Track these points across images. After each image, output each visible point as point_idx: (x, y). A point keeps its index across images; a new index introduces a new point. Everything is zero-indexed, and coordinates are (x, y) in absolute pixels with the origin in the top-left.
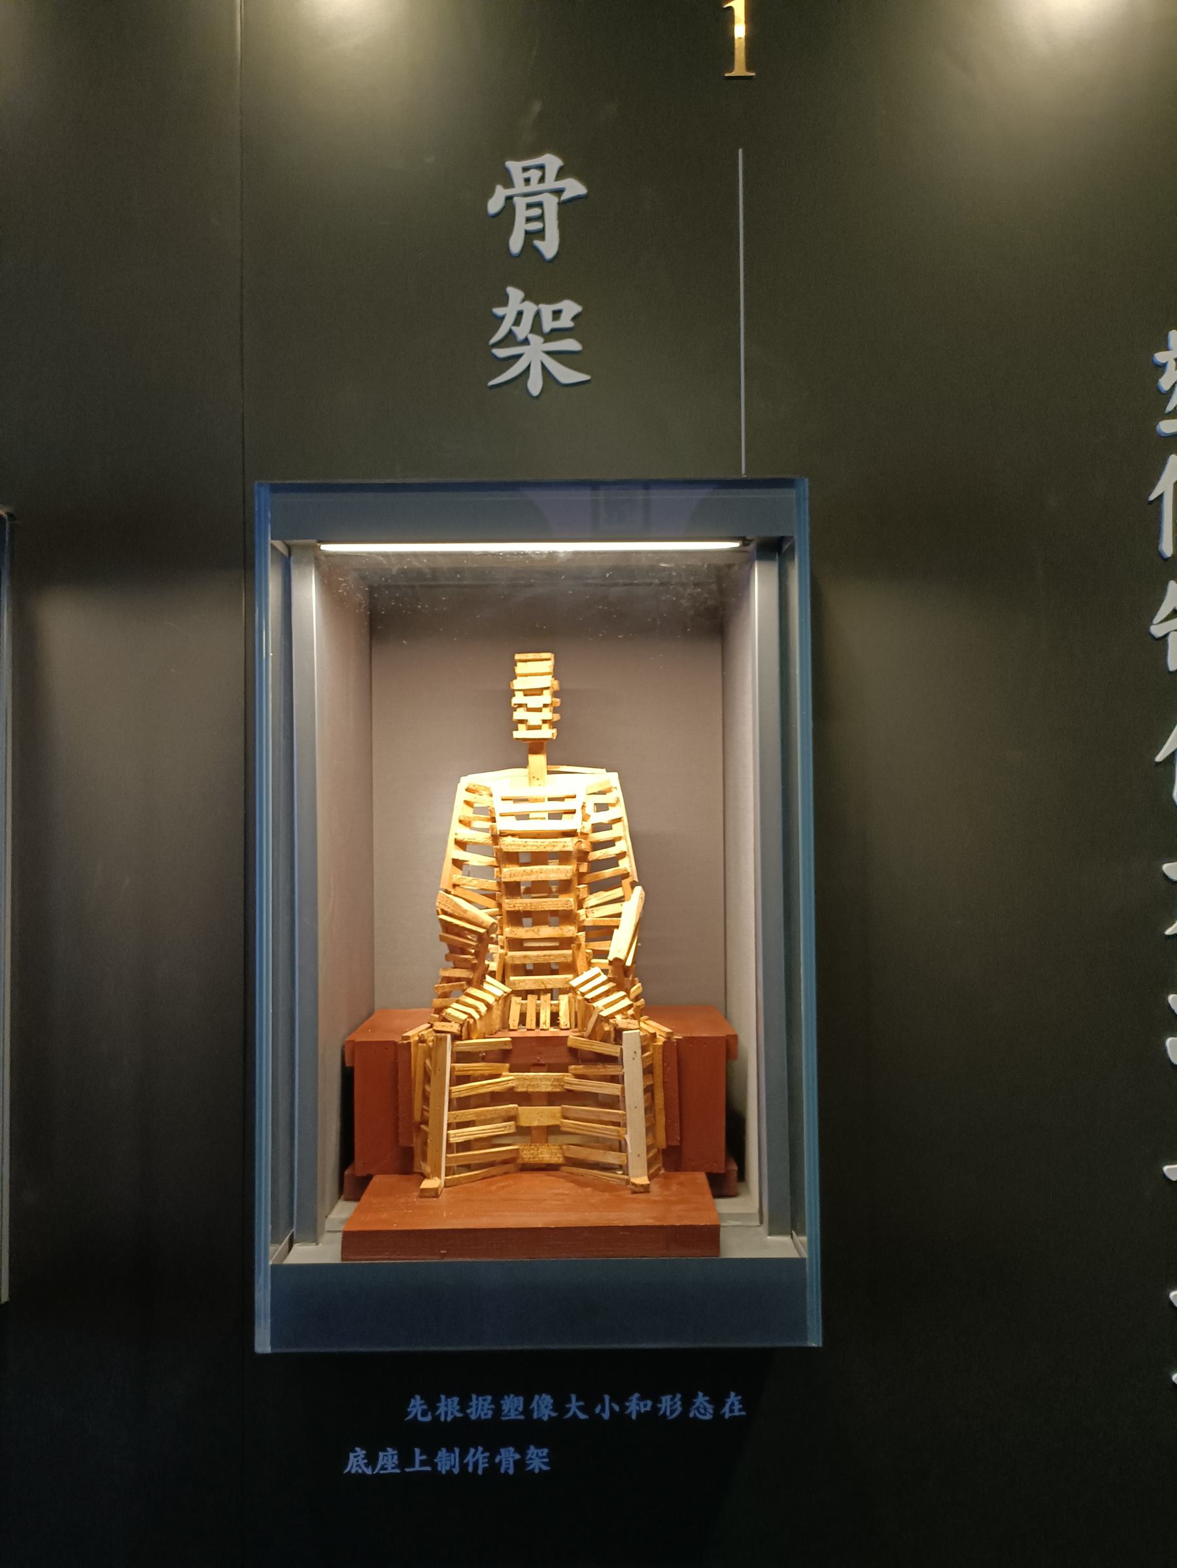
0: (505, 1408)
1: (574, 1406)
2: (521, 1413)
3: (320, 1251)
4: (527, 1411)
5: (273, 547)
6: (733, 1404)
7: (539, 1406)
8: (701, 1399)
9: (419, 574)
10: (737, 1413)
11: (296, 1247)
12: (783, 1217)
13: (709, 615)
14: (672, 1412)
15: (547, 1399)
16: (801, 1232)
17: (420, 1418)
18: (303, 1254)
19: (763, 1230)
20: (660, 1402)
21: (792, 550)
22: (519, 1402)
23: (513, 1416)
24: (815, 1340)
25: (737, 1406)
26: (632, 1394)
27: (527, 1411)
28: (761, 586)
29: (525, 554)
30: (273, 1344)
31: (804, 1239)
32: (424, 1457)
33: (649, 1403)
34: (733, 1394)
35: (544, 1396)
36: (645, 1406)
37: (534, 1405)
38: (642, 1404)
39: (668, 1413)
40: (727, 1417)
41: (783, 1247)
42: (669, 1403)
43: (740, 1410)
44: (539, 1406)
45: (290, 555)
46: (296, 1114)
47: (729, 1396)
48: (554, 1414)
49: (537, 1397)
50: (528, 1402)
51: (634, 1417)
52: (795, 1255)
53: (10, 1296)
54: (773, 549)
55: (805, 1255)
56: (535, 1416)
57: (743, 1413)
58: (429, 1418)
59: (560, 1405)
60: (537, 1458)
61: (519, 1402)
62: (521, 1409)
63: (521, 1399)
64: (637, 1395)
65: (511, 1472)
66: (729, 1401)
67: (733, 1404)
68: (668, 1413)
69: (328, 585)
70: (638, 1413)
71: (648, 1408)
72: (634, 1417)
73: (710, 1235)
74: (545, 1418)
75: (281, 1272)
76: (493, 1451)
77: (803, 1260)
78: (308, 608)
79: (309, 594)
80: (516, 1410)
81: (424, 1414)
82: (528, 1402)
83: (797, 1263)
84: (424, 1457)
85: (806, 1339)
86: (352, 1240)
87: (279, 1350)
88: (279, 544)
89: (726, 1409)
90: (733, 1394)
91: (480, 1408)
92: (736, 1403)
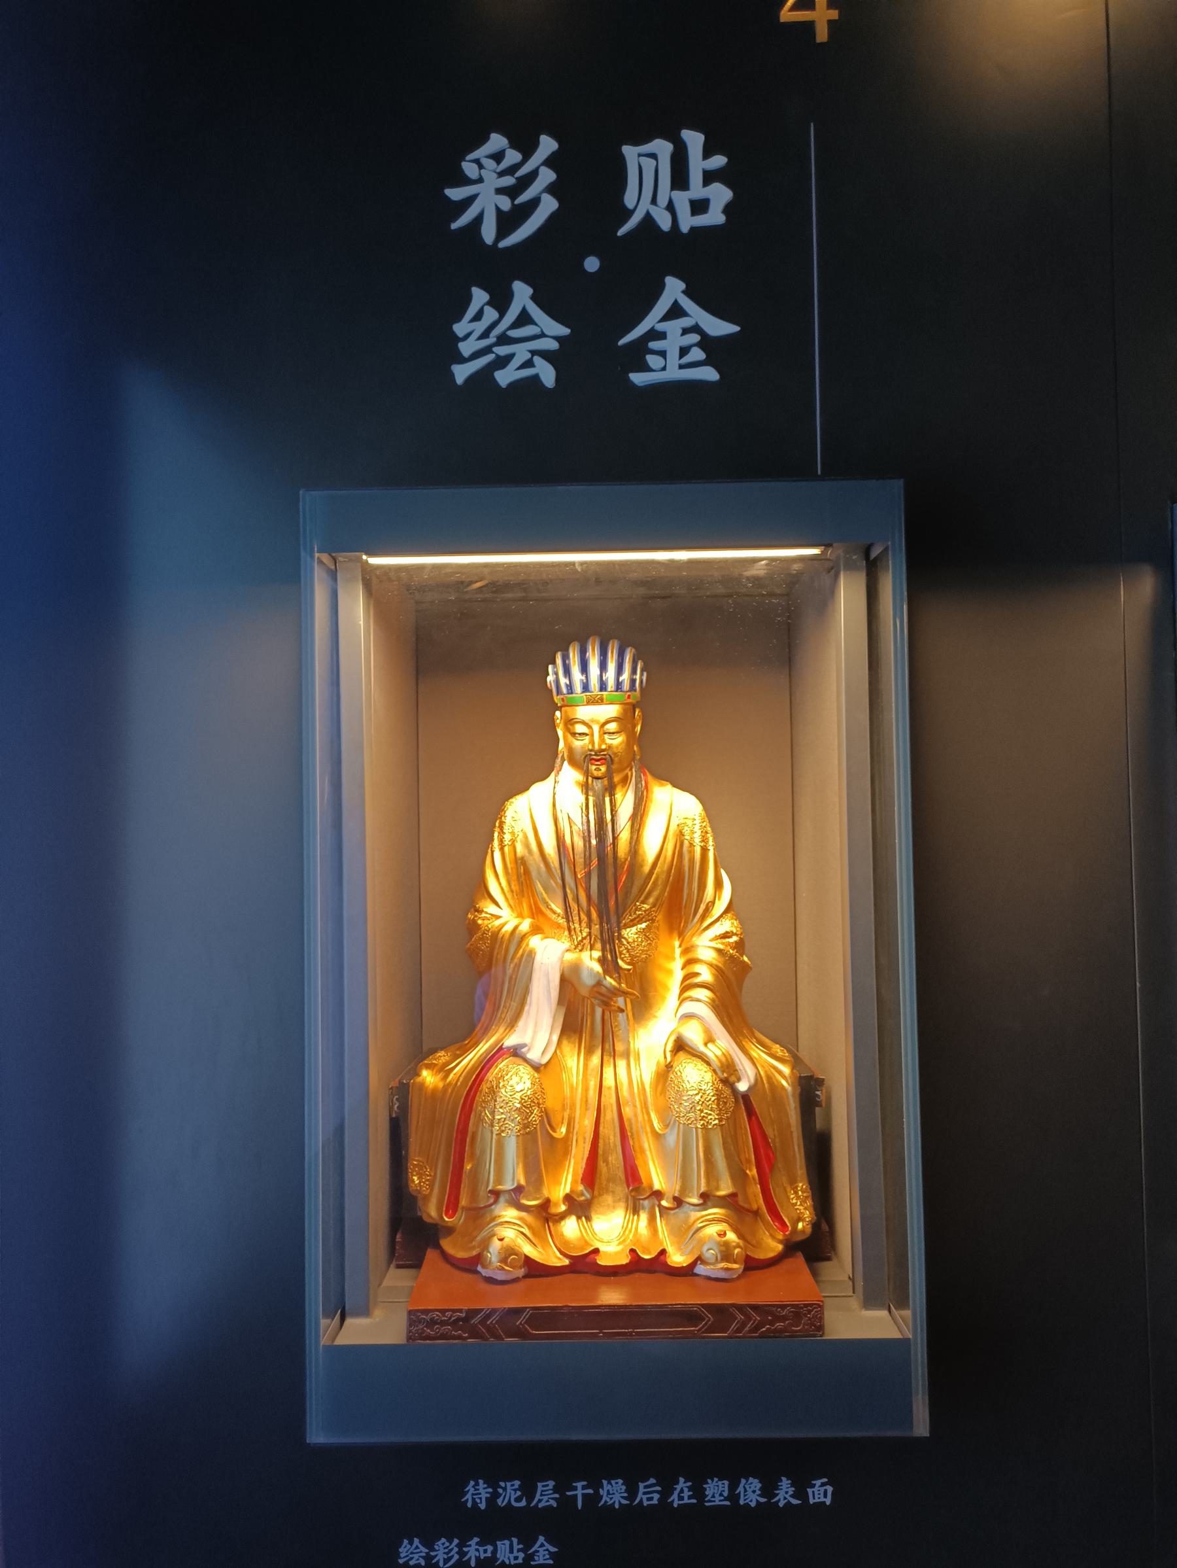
1: (785, 1493)
2: (726, 1499)
3: (377, 1326)
4: (733, 1497)
5: (320, 562)
6: (682, 1491)
7: (745, 1491)
8: (785, 1483)
10: (686, 1501)
11: (349, 1321)
12: (881, 1289)
13: (772, 629)
15: (755, 1484)
16: (902, 1303)
19: (854, 1303)
23: (717, 1501)
24: (921, 1427)
25: (686, 1494)
27: (733, 1497)
28: (848, 596)
29: (573, 564)
31: (907, 1313)
32: (521, 1546)
34: (682, 1480)
35: (751, 1479)
36: (485, 1551)
37: (740, 1489)
38: (481, 1549)
40: (675, 1505)
43: (690, 1497)
44: (745, 1491)
47: (677, 1483)
48: (763, 1500)
49: (743, 1481)
50: (733, 1487)
51: (473, 1564)
52: (896, 1335)
56: (742, 1502)
57: (694, 1501)
58: (523, 1503)
59: (769, 1490)
62: (726, 1494)
63: (726, 1482)
64: (476, 1540)
66: (678, 1487)
67: (682, 1491)
72: (473, 1564)
73: (809, 1316)
74: (753, 1504)
76: (528, 1542)
79: (357, 613)
81: (518, 1500)
82: (733, 1487)
84: (521, 1546)
88: (325, 558)
89: (675, 1496)
90: (682, 1480)
92: (686, 1490)
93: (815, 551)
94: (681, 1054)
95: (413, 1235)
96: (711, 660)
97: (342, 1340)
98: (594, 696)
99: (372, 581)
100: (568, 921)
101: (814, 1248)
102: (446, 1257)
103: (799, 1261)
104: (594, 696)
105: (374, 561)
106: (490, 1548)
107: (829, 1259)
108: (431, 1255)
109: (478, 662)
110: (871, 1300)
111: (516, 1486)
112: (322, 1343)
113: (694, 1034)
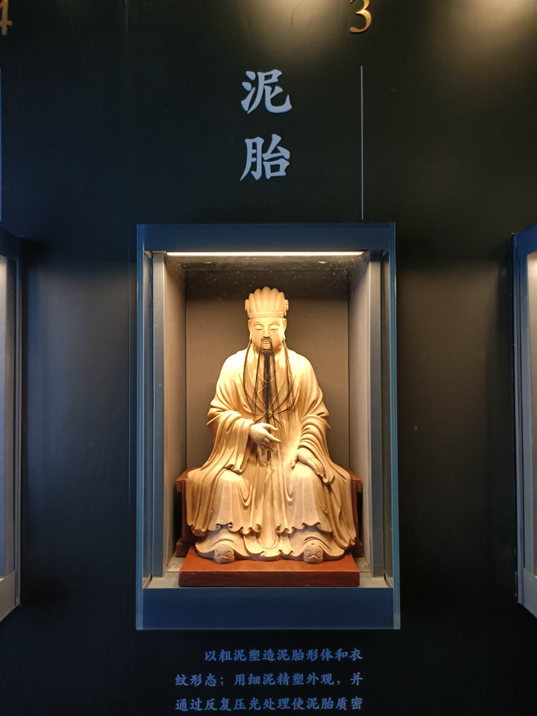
0: (251, 655)
5: (145, 254)
9: (232, 265)
11: (154, 579)
14: (313, 658)
17: (284, 659)
18: (158, 583)
19: (370, 575)
20: (308, 653)
21: (387, 256)
22: (258, 652)
24: (397, 626)
26: (338, 649)
28: (372, 274)
30: (144, 627)
31: (392, 579)
33: (347, 653)
34: (210, 674)
36: (345, 654)
38: (343, 653)
39: (311, 658)
41: (379, 583)
42: (312, 654)
45: (152, 257)
46: (152, 519)
47: (208, 676)
50: (262, 653)
51: (339, 659)
53: (21, 603)
54: (379, 257)
55: (393, 587)
60: (180, 680)
61: (258, 652)
64: (341, 649)
65: (287, 684)
68: (311, 658)
69: (170, 272)
70: (341, 657)
71: (346, 656)
72: (339, 659)
75: (148, 592)
77: (392, 589)
78: (159, 283)
79: (161, 273)
80: (256, 656)
82: (262, 653)
83: (389, 591)
85: (393, 626)
86: (185, 578)
87: (145, 629)
88: (147, 252)
90: (210, 674)
91: (312, 655)
93: (360, 253)
94: (298, 462)
95: (186, 539)
96: (318, 298)
97: (152, 586)
98: (267, 311)
99: (167, 260)
100: (267, 408)
101: (355, 551)
102: (196, 551)
103: (350, 558)
104: (267, 311)
105: (170, 254)
106: (347, 653)
107: (361, 557)
108: (191, 551)
109: (214, 295)
110: (376, 573)
111: (242, 652)
112: (143, 588)
113: (305, 454)
